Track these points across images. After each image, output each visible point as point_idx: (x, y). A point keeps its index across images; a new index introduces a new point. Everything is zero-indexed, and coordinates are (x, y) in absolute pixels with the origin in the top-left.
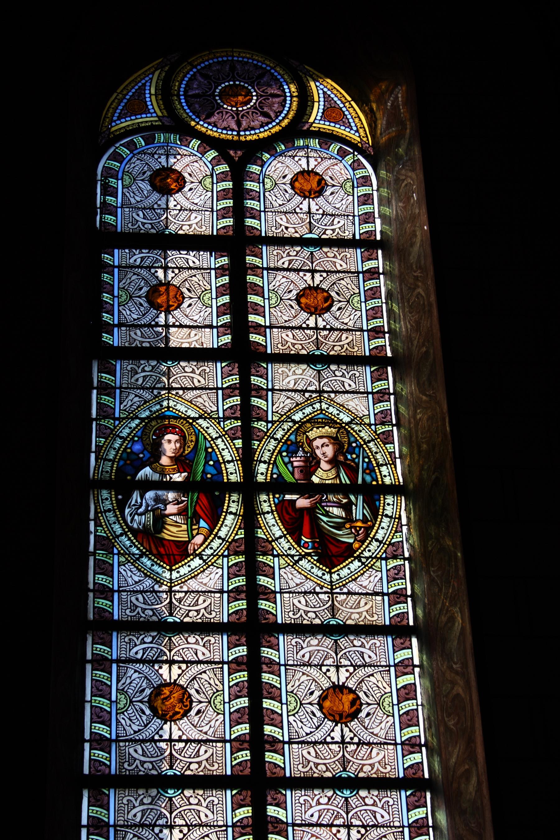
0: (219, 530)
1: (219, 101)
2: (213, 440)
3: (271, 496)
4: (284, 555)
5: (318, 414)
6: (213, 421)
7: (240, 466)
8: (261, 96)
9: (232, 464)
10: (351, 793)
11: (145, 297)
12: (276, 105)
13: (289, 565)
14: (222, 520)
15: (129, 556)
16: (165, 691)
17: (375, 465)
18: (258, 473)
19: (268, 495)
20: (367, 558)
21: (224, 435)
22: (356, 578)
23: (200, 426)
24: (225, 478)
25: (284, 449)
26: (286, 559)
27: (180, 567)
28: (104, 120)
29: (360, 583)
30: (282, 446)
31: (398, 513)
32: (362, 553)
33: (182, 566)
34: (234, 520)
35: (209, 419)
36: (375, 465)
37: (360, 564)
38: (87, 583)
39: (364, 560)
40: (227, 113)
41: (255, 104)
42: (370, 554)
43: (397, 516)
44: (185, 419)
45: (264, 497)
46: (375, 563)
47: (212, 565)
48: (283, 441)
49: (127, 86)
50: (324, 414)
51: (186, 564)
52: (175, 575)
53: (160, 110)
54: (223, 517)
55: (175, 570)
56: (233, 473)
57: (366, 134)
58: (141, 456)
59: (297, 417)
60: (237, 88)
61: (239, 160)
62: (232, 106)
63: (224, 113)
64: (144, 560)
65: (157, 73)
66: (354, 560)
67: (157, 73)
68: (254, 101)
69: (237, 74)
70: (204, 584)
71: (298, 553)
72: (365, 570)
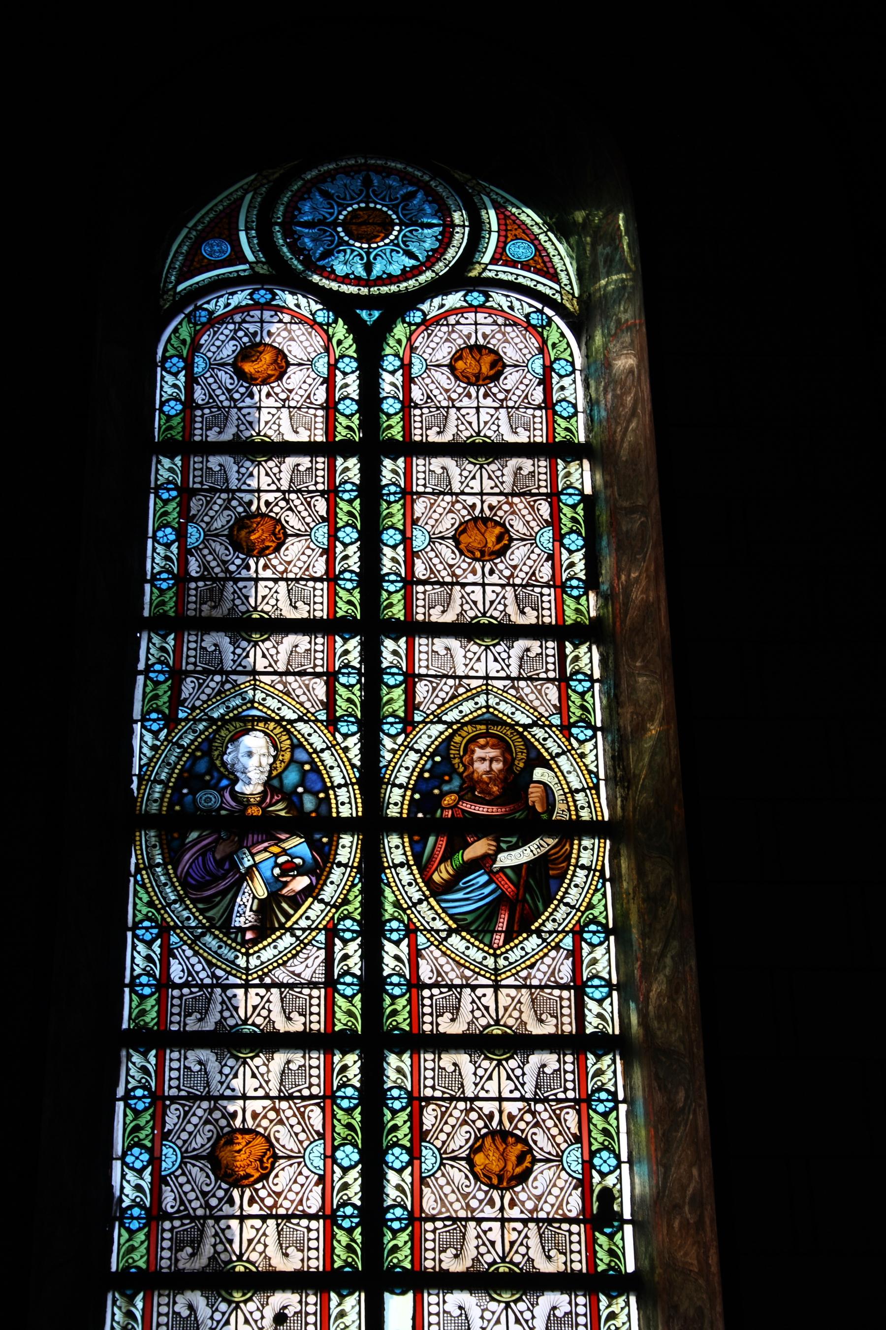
1: (342, 234)
2: (315, 751)
3: (406, 840)
4: (425, 929)
5: (483, 714)
6: (319, 724)
7: (357, 792)
10: (244, 1295)
12: (429, 241)
13: (432, 943)
14: (569, 877)
15: (182, 931)
16: (240, 1141)
18: (389, 803)
19: (402, 838)
21: (569, 751)
22: (285, 963)
24: (334, 810)
25: (428, 766)
26: (428, 936)
27: (260, 949)
29: (291, 969)
30: (426, 762)
31: (600, 863)
32: (543, 924)
33: (264, 948)
34: (587, 876)
35: (313, 721)
37: (540, 941)
38: (124, 977)
41: (397, 237)
42: (310, 922)
43: (599, 868)
44: (512, 726)
45: (395, 840)
46: (561, 940)
48: (428, 754)
49: (203, 217)
50: (492, 713)
51: (516, 946)
53: (253, 252)
55: (253, 954)
56: (347, 804)
57: (570, 279)
58: (208, 778)
59: (452, 716)
61: (371, 323)
63: (348, 251)
64: (208, 938)
65: (249, 197)
66: (284, 934)
67: (249, 197)
69: (374, 191)
70: (287, 976)
71: (446, 927)
72: (298, 949)
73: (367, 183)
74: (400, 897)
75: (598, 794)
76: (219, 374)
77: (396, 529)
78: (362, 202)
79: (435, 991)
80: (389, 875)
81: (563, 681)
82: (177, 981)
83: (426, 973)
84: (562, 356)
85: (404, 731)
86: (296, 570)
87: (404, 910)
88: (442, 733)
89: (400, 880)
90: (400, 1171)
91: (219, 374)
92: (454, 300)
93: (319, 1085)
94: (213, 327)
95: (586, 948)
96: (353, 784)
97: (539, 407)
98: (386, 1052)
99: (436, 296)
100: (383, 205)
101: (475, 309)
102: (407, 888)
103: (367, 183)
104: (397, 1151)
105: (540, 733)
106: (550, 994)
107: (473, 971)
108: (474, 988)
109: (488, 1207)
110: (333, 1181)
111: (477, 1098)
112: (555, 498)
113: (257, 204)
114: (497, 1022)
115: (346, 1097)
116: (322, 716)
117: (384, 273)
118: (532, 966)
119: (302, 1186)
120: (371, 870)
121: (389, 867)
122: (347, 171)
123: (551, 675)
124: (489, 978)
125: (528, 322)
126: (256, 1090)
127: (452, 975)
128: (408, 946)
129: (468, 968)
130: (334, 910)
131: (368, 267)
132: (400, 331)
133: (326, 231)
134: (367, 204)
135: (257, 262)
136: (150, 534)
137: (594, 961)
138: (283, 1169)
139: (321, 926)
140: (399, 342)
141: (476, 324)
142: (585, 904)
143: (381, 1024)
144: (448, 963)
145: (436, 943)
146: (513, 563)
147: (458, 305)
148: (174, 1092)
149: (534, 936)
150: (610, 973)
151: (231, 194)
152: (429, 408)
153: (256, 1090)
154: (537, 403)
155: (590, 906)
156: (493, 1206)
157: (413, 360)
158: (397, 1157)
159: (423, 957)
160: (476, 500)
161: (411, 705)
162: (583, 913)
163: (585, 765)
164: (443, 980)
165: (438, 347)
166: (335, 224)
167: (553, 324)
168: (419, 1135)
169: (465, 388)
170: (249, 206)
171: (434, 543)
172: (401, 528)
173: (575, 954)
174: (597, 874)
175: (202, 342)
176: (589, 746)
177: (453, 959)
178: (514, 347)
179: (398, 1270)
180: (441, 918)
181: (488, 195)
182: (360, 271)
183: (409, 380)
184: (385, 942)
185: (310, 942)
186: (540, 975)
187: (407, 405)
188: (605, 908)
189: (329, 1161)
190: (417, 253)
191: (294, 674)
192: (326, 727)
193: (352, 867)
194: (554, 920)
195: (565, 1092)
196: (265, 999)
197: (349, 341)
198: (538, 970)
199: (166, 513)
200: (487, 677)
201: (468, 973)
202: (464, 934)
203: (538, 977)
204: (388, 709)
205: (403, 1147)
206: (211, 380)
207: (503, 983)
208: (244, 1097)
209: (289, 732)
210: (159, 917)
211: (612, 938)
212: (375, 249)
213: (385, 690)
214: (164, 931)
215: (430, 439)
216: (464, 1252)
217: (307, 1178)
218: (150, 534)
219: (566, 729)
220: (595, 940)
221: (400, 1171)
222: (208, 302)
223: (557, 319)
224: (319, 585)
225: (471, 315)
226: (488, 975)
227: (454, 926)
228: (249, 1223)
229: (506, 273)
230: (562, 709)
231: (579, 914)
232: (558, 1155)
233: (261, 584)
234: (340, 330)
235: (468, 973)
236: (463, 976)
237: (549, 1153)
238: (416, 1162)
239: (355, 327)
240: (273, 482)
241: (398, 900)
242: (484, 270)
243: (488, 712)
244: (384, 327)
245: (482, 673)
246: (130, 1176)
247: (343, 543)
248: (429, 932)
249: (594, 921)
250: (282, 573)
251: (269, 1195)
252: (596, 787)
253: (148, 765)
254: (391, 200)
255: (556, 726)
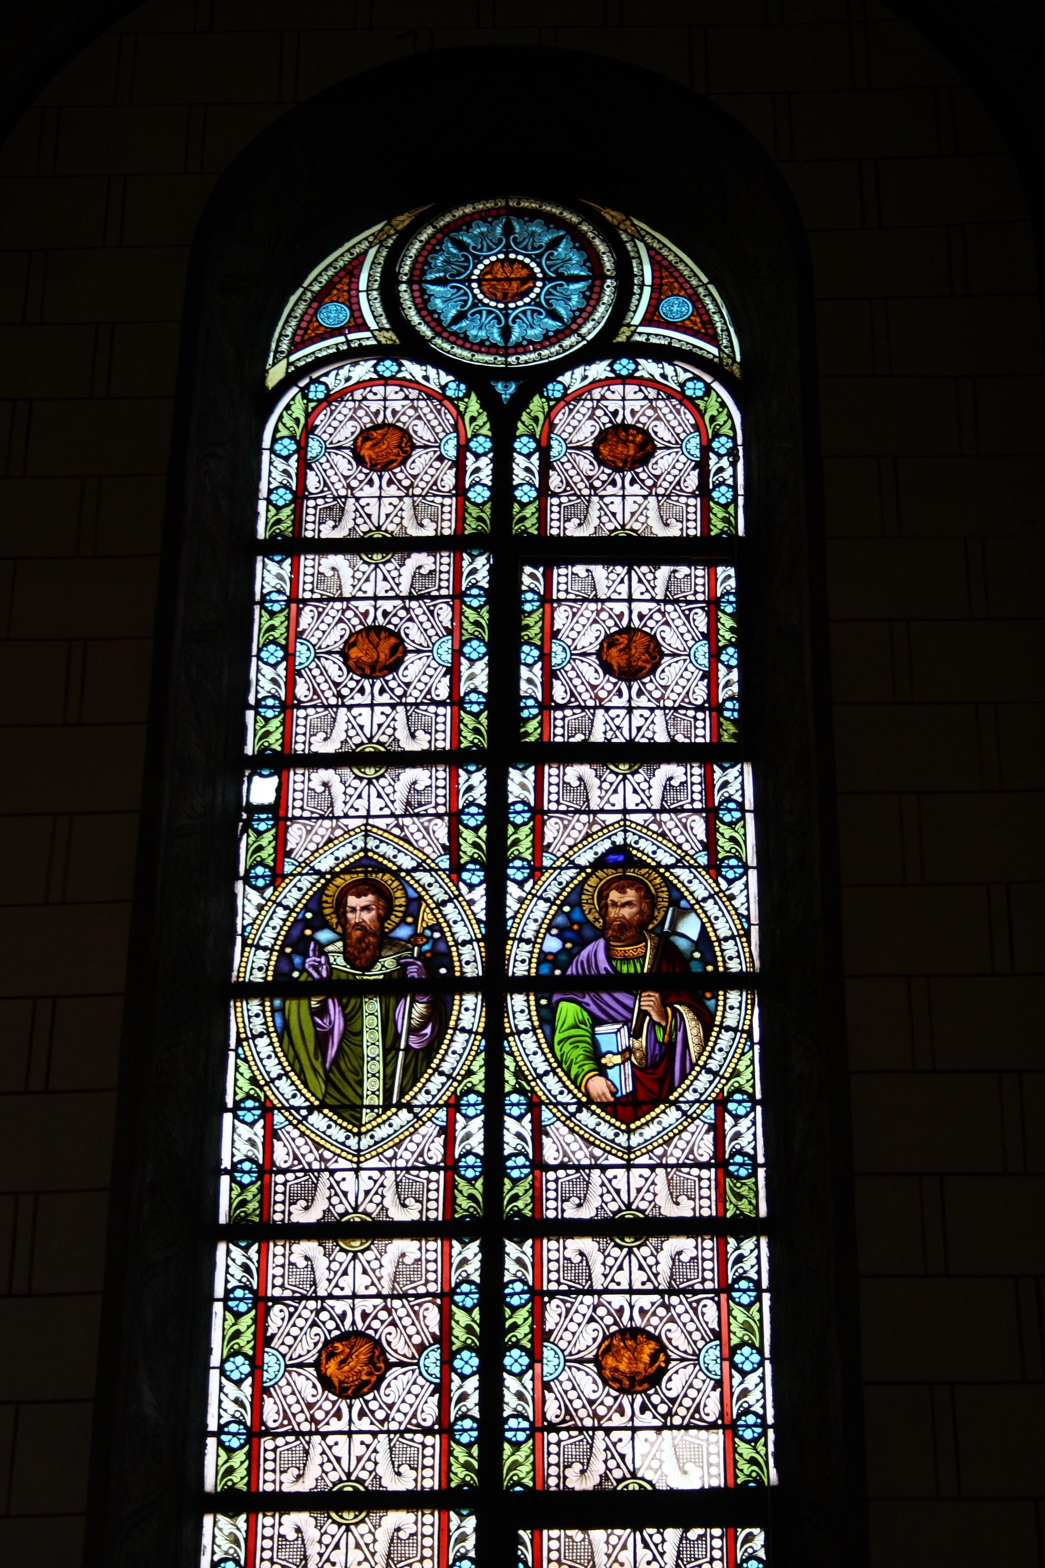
0: (442, 1060)
4: (283, 1107)
8: (462, 282)
9: (469, 946)
11: (663, 655)
17: (451, 943)
20: (422, 1107)
23: (417, 882)
28: (279, 341)
31: (747, 1022)
36: (451, 943)
39: (416, 1110)
40: (489, 313)
41: (538, 295)
43: (746, 1028)
47: (430, 1119)
52: (635, 1140)
54: (448, 1037)
55: (634, 1131)
56: (470, 961)
60: (511, 266)
62: (498, 302)
63: (484, 314)
65: (372, 252)
67: (372, 252)
68: (537, 290)
73: (508, 230)
74: (257, 1073)
75: (749, 942)
76: (578, 458)
77: (278, 644)
78: (500, 252)
79: (561, 1173)
80: (513, 1044)
81: (711, 814)
82: (551, 1162)
83: (550, 1155)
84: (722, 432)
85: (531, 876)
86: (416, 693)
87: (261, 1088)
88: (573, 879)
89: (258, 1053)
90: (520, 1376)
91: (578, 458)
92: (599, 370)
93: (436, 1281)
94: (568, 403)
95: (729, 1121)
96: (478, 941)
97: (693, 495)
98: (507, 1242)
99: (578, 366)
100: (525, 256)
101: (385, 381)
102: (265, 1062)
103: (508, 230)
104: (515, 1353)
105: (684, 874)
106: (689, 1173)
107: (604, 1150)
108: (604, 1168)
109: (335, 1419)
110: (731, 1387)
111: (606, 1291)
112: (457, 601)
113: (381, 260)
114: (355, 1210)
115: (518, 1294)
116: (703, 860)
117: (524, 339)
118: (667, 1143)
119: (417, 1396)
120: (495, 1036)
121: (512, 1034)
122: (482, 216)
123: (698, 805)
124: (621, 1158)
125: (683, 392)
126: (367, 1288)
127: (580, 1155)
128: (264, 1127)
129: (598, 1146)
130: (455, 1084)
131: (506, 332)
132: (537, 405)
133: (459, 289)
134: (507, 254)
135: (380, 329)
136: (254, 651)
137: (737, 1135)
138: (676, 1372)
139: (441, 1102)
140: (536, 419)
141: (385, 399)
142: (730, 1070)
143: (502, 1211)
144: (576, 1141)
145: (563, 1119)
146: (406, 680)
147: (367, 378)
148: (553, 1286)
149: (316, 1113)
150: (755, 1148)
151: (354, 247)
152: (324, 497)
153: (367, 1288)
154: (690, 490)
155: (736, 1073)
156: (622, 1414)
157: (552, 443)
158: (516, 1360)
159: (547, 1135)
160: (622, 607)
161: (539, 847)
162: (728, 1080)
163: (474, 914)
164: (570, 1160)
165: (580, 426)
166: (546, 279)
167: (713, 393)
168: (541, 1335)
169: (367, 475)
170: (373, 263)
171: (319, 658)
172: (283, 642)
173: (717, 1128)
174: (745, 1036)
175: (317, 422)
176: (738, 886)
177: (582, 1137)
178: (667, 424)
179: (518, 1489)
180: (302, 1095)
181: (643, 240)
182: (496, 337)
183: (546, 466)
184: (506, 1118)
185: (430, 1119)
186: (677, 1153)
187: (544, 492)
188: (750, 1074)
189: (726, 1364)
190: (563, 312)
191: (669, 811)
192: (448, 876)
193: (477, 1033)
194: (428, 1092)
195: (702, 1282)
196: (650, 1181)
197: (484, 417)
198: (676, 1147)
199: (272, 628)
200: (625, 811)
201: (598, 1152)
202: (326, 1111)
203: (675, 1155)
204: (513, 851)
205: (522, 1348)
206: (568, 466)
207: (637, 1162)
208: (631, 1291)
209: (666, 880)
210: (262, 1095)
211: (759, 1109)
212: (514, 309)
213: (511, 829)
214: (267, 1110)
215: (568, 533)
216: (592, 1467)
217: (422, 1387)
218: (254, 651)
219: (714, 868)
220: (741, 1111)
221: (520, 1376)
222: (326, 374)
223: (716, 386)
224: (441, 710)
225: (619, 388)
226: (620, 1154)
227: (317, 1103)
228: (357, 1438)
229: (659, 335)
230: (710, 845)
231: (724, 1081)
232: (694, 1354)
233: (378, 710)
234: (474, 406)
235: (598, 1152)
236: (592, 1156)
237: (685, 1352)
238: (537, 1366)
239: (489, 402)
240: (647, 591)
241: (254, 1076)
242: (634, 332)
243: (366, 856)
244: (521, 402)
245: (619, 806)
246: (229, 1387)
247: (469, 659)
248: (288, 1109)
249: (739, 1090)
250: (400, 697)
251: (662, 1402)
252: (747, 934)
253: (252, 924)
254: (534, 249)
255: (444, 870)
